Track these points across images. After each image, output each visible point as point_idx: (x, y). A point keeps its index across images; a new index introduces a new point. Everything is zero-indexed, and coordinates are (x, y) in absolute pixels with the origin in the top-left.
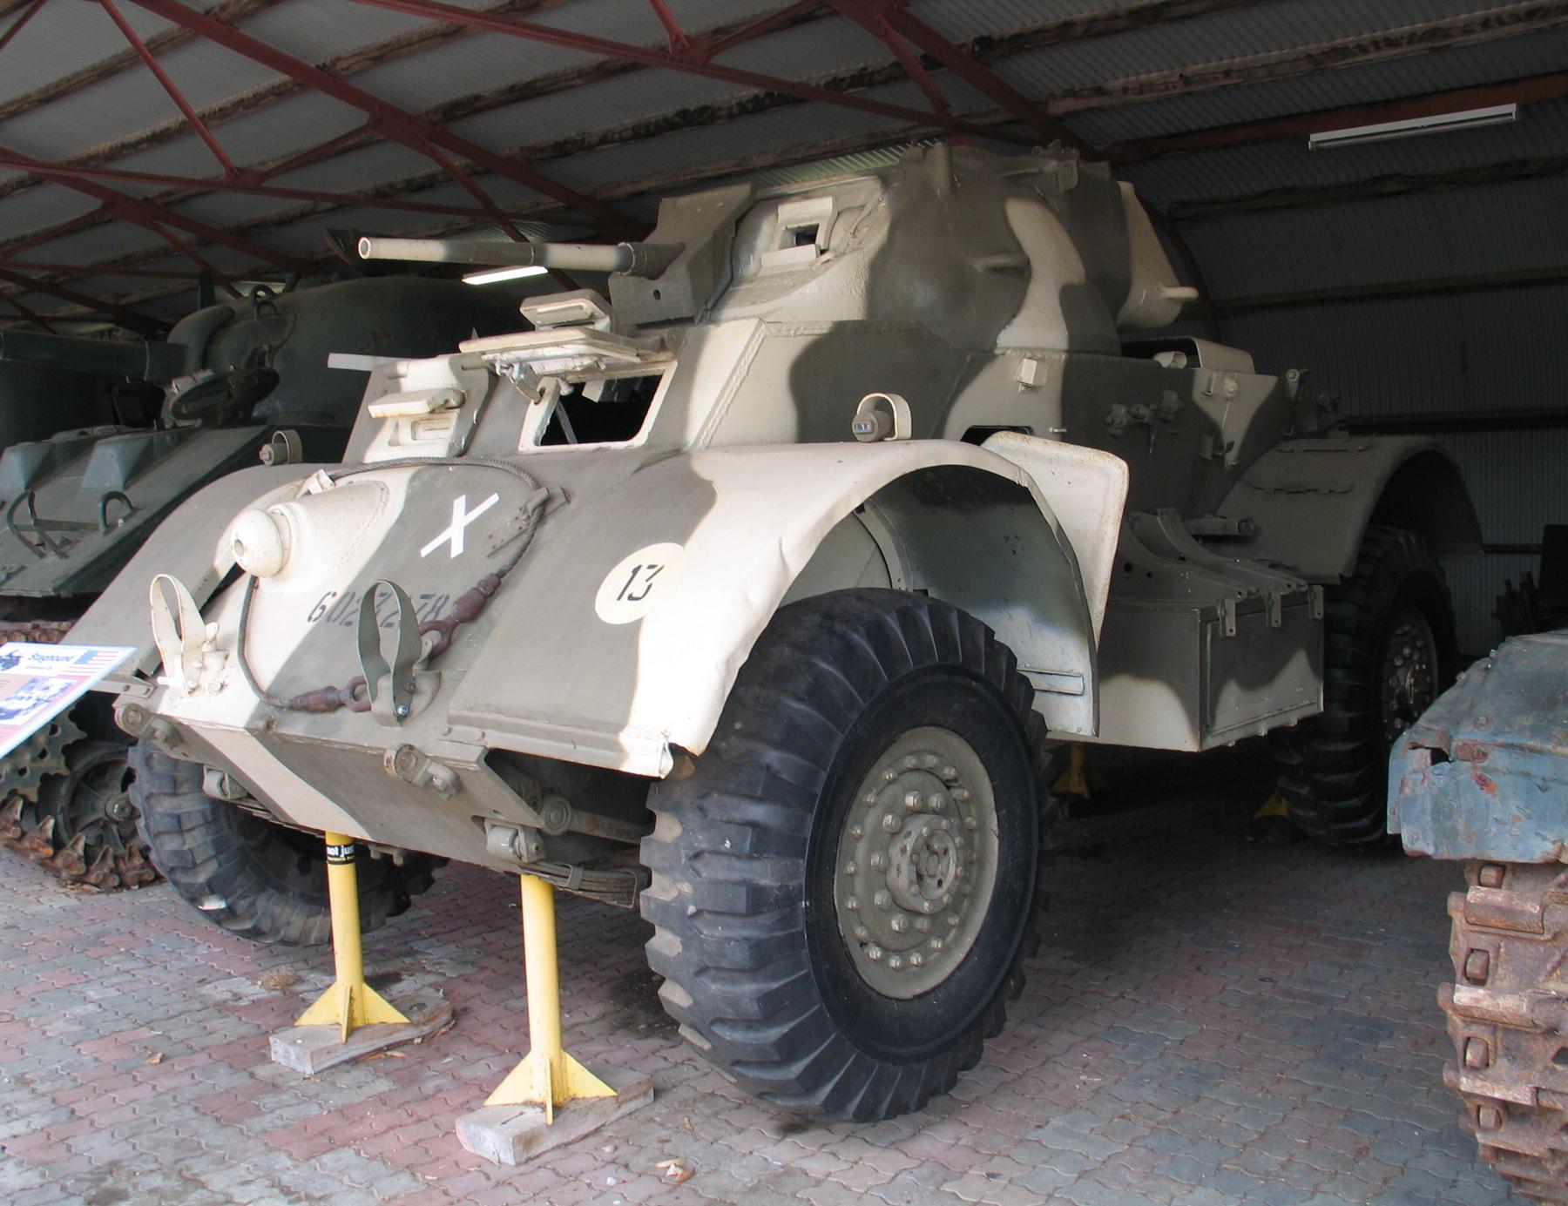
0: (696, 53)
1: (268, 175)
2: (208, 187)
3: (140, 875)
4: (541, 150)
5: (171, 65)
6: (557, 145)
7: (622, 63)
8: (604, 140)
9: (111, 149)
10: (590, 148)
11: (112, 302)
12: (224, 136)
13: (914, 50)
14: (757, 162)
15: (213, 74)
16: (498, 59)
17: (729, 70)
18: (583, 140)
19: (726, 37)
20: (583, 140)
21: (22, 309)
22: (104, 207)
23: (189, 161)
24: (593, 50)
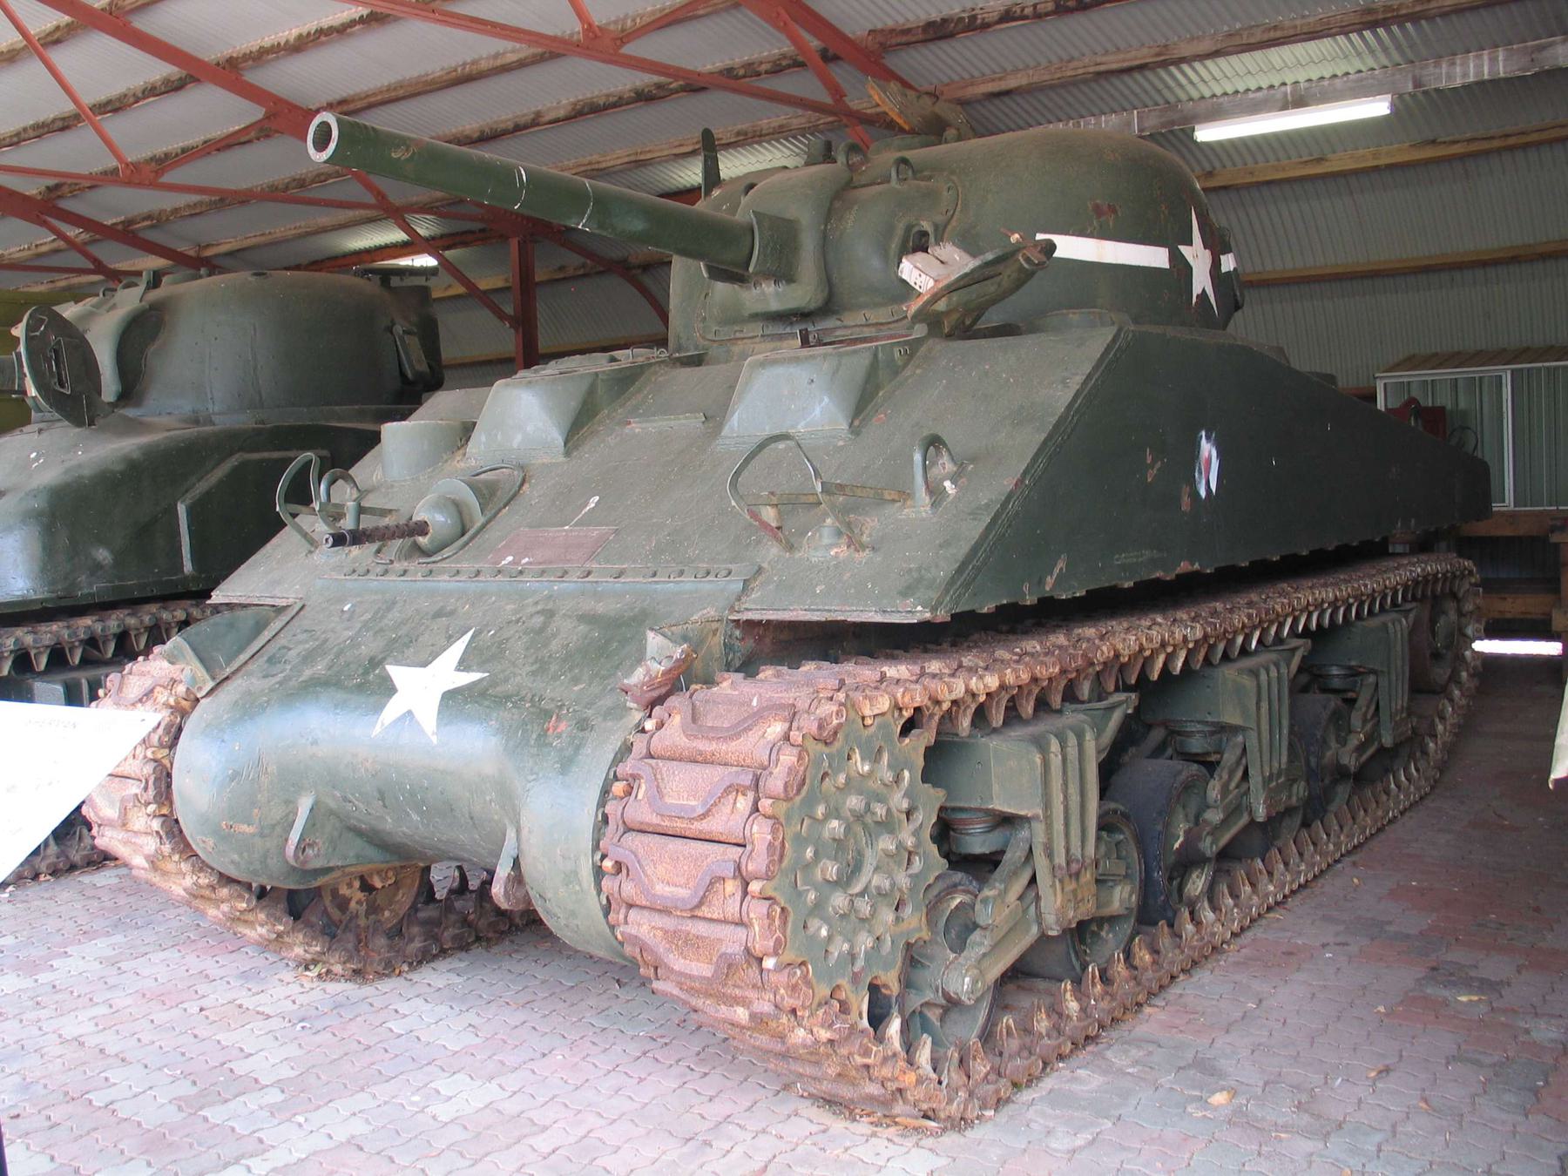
0: (600, 43)
1: (626, 37)
2: (96, 182)
3: (55, 864)
4: (908, 31)
5: (61, 57)
6: (930, 25)
7: (550, 50)
8: (1007, 16)
9: (300, 36)
10: (986, 26)
11: (192, 253)
12: (115, 126)
13: (815, 43)
14: (1186, 50)
15: (103, 66)
16: (416, 47)
17: (643, 61)
18: (974, 17)
19: (164, 162)
20: (974, 17)
21: (95, 261)
22: (267, 117)
23: (76, 154)
24: (505, 37)
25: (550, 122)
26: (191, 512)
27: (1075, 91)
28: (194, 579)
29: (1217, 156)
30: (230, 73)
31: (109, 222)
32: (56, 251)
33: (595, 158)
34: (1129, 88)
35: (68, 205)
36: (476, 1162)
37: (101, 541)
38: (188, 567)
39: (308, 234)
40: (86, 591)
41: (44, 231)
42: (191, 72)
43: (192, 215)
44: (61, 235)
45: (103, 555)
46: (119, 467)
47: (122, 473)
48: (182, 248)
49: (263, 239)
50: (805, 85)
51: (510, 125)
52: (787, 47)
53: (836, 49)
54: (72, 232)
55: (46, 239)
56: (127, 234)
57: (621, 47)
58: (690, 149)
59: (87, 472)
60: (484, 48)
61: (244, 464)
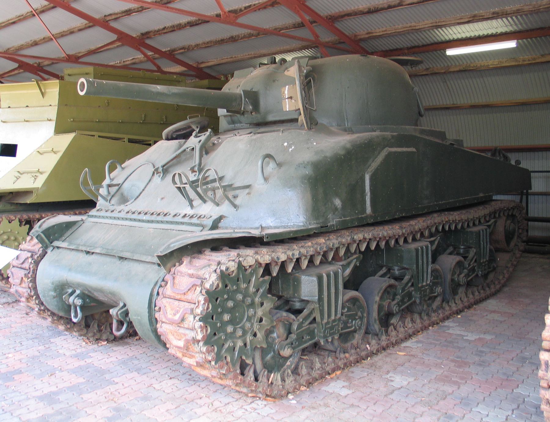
7: (201, 21)
11: (195, 65)
12: (62, 41)
13: (307, 18)
15: (60, 20)
16: (155, 19)
21: (158, 67)
25: (409, 5)
26: (371, 179)
27: (396, 37)
28: (371, 216)
29: (453, 61)
30: (104, 23)
31: (164, 50)
32: (141, 62)
33: (413, 24)
34: (420, 36)
35: (148, 42)
36: (161, 382)
37: (337, 195)
38: (369, 210)
39: (251, 58)
40: (331, 223)
41: (139, 52)
42: (93, 22)
43: (206, 47)
44: (145, 55)
45: (338, 202)
46: (342, 152)
47: (344, 155)
48: (191, 63)
49: (231, 59)
50: (304, 33)
51: (386, 6)
52: (298, 20)
53: (317, 19)
54: (150, 53)
55: (140, 56)
56: (171, 55)
57: (237, 18)
58: (467, 20)
59: (329, 154)
60: (184, 19)
61: (390, 154)
